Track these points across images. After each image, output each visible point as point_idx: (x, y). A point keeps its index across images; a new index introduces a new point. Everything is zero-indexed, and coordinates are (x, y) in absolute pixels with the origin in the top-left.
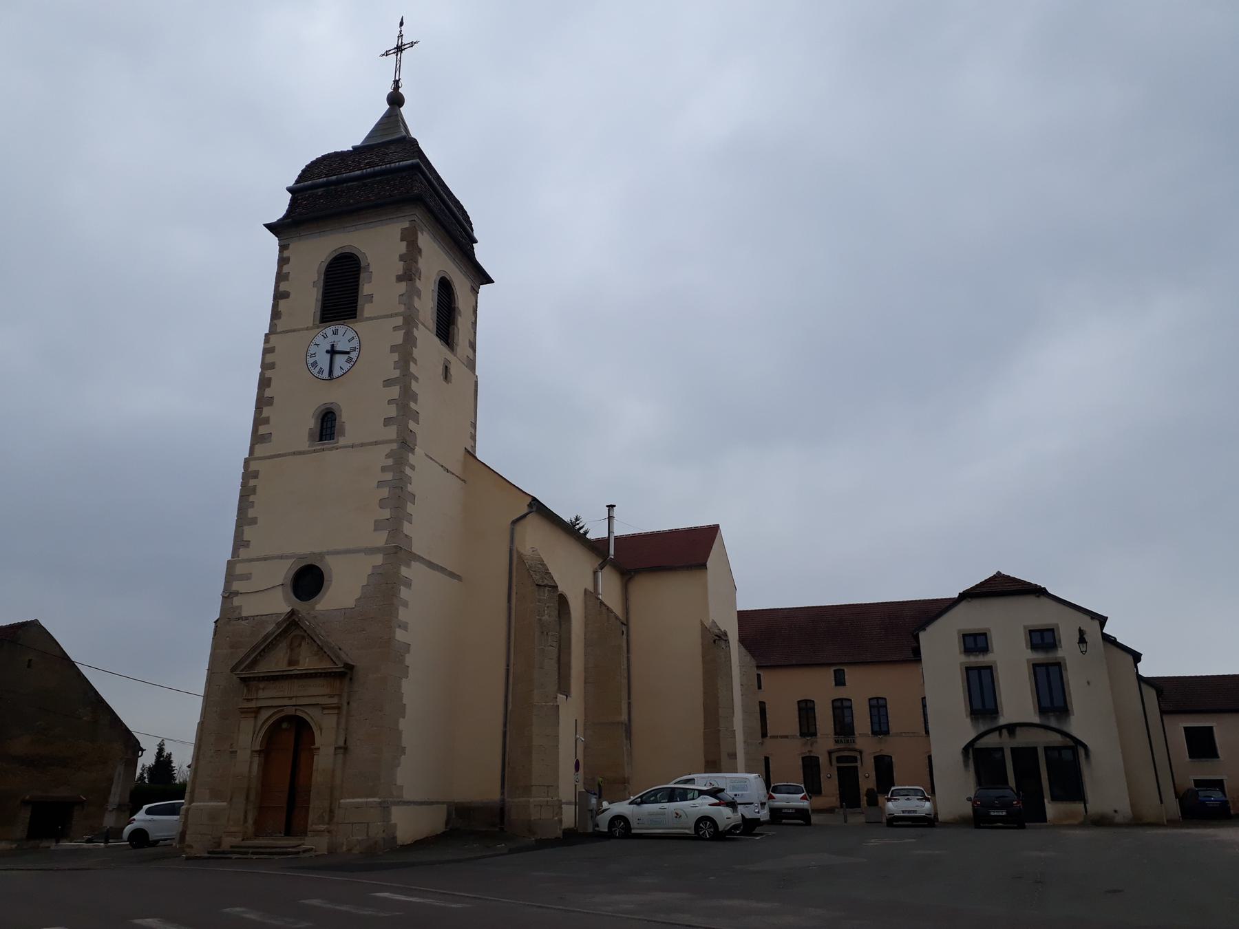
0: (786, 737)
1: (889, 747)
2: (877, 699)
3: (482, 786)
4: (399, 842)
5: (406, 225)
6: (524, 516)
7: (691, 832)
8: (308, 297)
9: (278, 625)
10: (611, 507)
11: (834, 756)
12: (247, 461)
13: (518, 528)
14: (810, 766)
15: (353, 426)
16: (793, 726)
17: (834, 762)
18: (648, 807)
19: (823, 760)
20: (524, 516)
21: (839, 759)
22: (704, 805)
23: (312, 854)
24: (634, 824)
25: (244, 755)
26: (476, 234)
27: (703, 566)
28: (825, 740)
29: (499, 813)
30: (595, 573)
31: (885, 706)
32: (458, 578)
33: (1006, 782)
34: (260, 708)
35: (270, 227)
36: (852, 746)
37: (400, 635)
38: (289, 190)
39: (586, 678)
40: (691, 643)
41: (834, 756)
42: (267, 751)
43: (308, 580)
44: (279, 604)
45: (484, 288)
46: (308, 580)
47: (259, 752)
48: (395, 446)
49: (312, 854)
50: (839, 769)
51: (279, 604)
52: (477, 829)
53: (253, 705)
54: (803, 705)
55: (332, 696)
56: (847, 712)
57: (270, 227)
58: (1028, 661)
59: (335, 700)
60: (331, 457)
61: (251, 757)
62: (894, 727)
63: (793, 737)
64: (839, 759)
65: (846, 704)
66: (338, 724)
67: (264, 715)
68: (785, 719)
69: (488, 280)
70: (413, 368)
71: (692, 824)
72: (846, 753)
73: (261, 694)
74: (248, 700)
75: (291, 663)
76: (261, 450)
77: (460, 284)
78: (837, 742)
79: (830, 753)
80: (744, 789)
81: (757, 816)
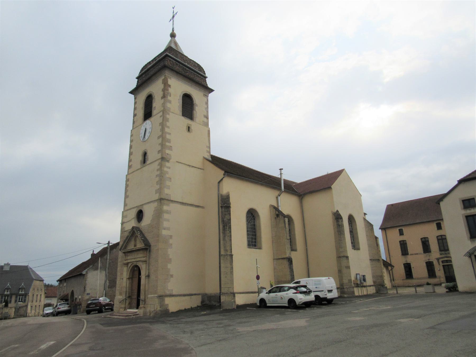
0: (417, 254)
1: (410, 259)
2: (441, 236)
3: (212, 288)
4: (170, 312)
5: (163, 78)
6: (222, 180)
7: (287, 305)
8: (141, 113)
9: (130, 232)
10: (281, 169)
11: (440, 260)
12: (127, 175)
13: (221, 184)
14: (430, 265)
15: (150, 158)
16: (420, 248)
17: (441, 263)
18: (272, 295)
19: (435, 263)
20: (222, 180)
21: (443, 262)
22: (291, 294)
23: (138, 316)
24: (267, 302)
25: (125, 280)
26: (207, 75)
27: (330, 188)
28: (435, 253)
29: (218, 298)
30: (277, 198)
31: (446, 239)
32: (203, 207)
33: (130, 308)
34: (129, 263)
35: (131, 93)
36: (448, 255)
37: (164, 232)
38: (137, 78)
39: (273, 241)
40: (329, 221)
41: (440, 260)
42: (131, 278)
43: (140, 215)
44: (133, 223)
45: (211, 95)
46: (140, 215)
47: (129, 278)
48: (160, 161)
49: (138, 316)
50: (443, 266)
51: (133, 223)
52: (211, 305)
53: (126, 262)
54: (402, 242)
55: (144, 257)
56: (427, 243)
57: (131, 93)
58: (462, 215)
59: (144, 259)
60: (146, 168)
61: (146, 279)
62: (410, 251)
63: (420, 254)
64: (443, 262)
65: (443, 237)
66: (146, 267)
67: (130, 265)
68: (415, 246)
69: (211, 91)
70: (167, 130)
71: (287, 302)
72: (446, 259)
73: (129, 258)
74: (125, 260)
75: (135, 246)
76: (131, 170)
77: (196, 94)
78: (441, 254)
79: (438, 259)
80: (320, 284)
81: (326, 296)
